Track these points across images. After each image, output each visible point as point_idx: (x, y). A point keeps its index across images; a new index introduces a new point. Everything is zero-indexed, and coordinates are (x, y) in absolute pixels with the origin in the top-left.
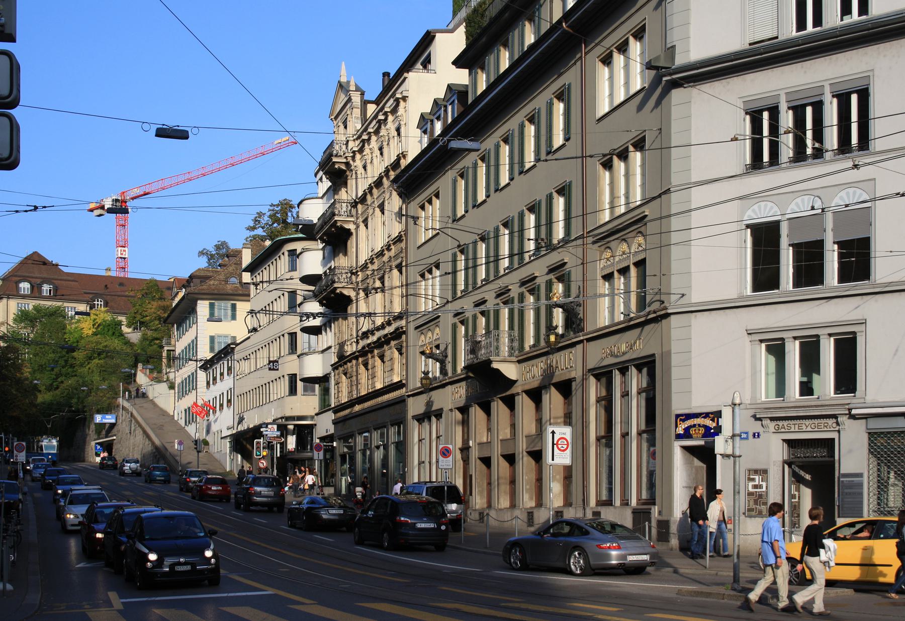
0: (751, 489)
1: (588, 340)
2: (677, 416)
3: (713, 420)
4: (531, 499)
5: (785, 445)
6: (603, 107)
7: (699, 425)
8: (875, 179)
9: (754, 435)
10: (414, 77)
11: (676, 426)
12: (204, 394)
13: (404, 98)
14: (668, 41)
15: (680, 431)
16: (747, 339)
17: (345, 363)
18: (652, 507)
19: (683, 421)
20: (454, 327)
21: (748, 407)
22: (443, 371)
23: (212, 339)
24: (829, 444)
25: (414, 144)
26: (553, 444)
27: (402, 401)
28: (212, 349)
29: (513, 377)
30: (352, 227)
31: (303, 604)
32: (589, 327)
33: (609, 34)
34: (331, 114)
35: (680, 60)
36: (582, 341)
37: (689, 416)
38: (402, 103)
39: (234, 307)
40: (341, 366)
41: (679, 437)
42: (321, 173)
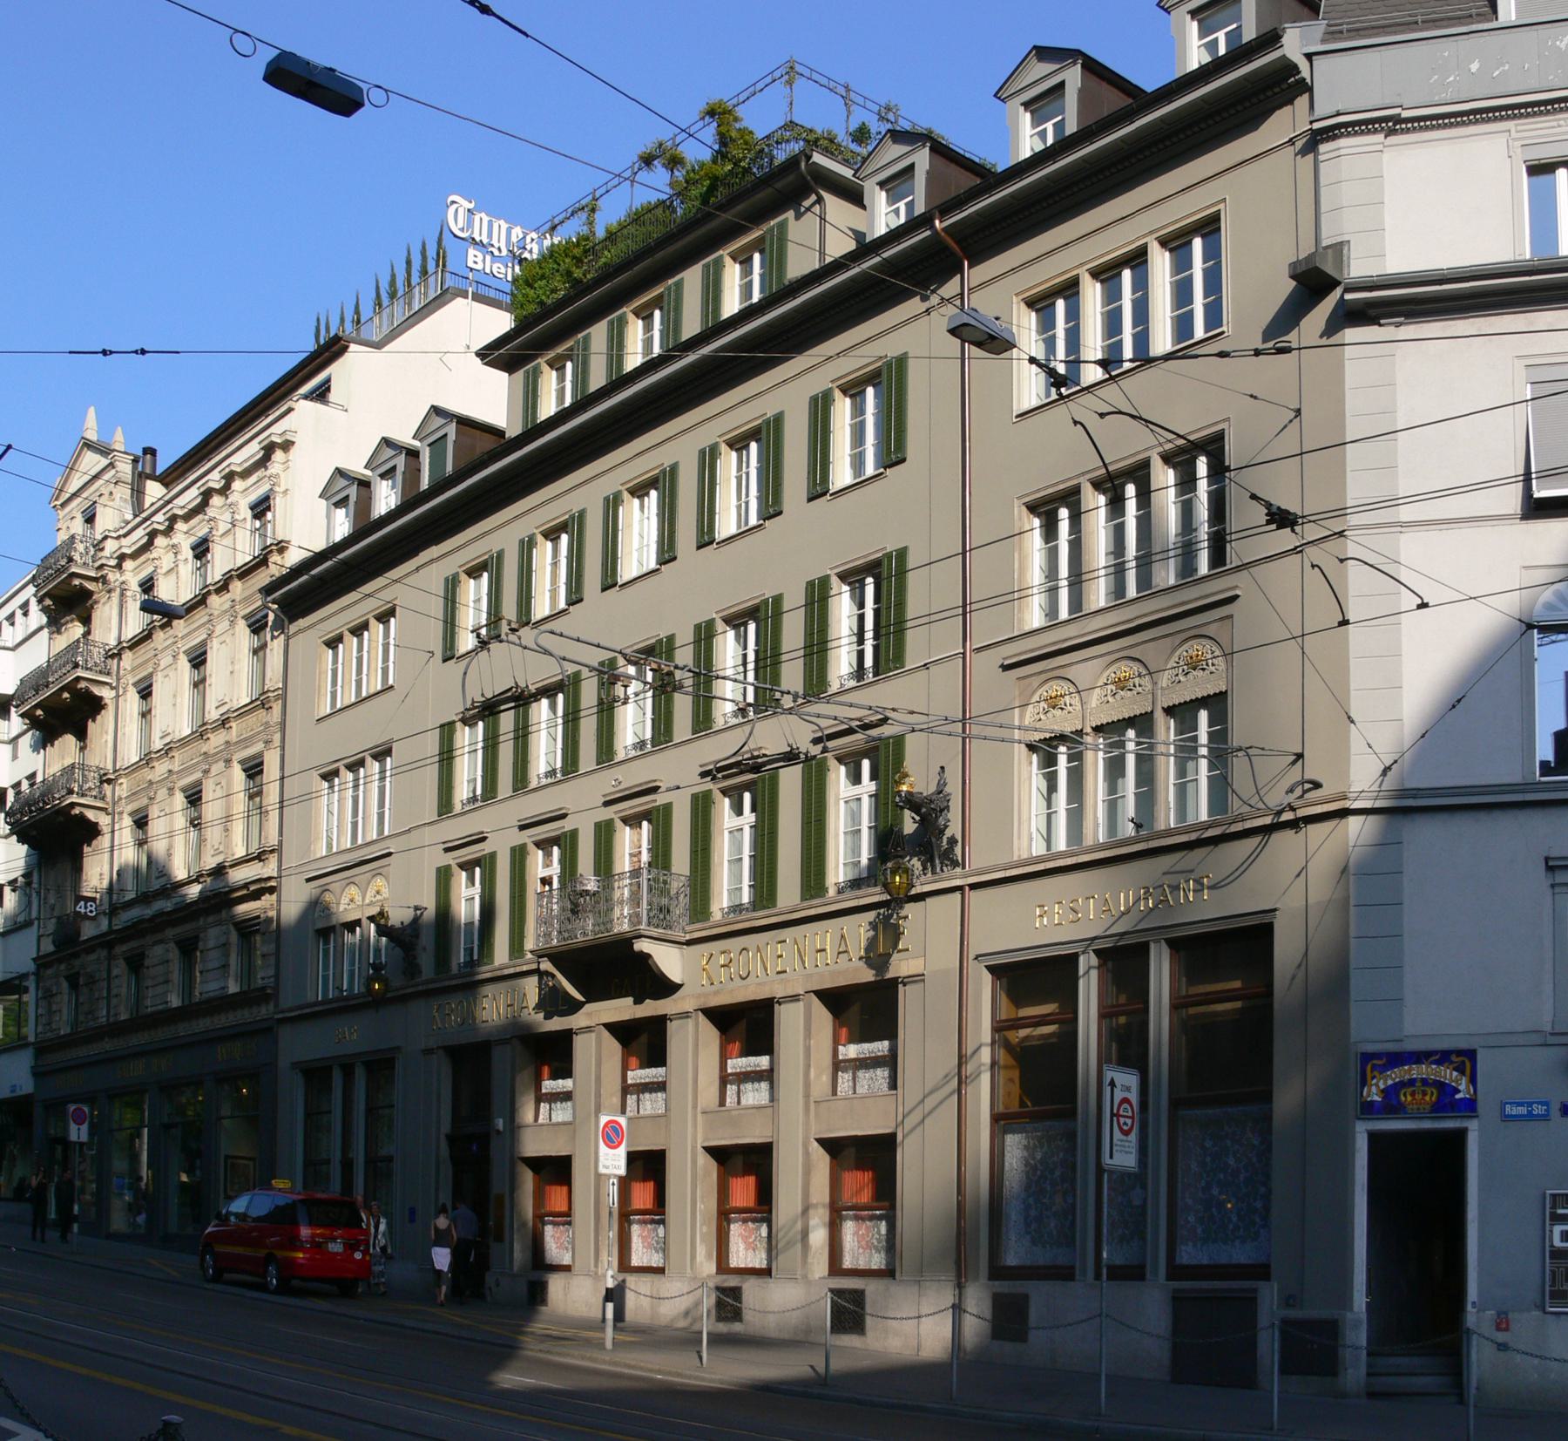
0: (1557, 1243)
1: (973, 887)
2: (1366, 1058)
3: (1460, 1069)
4: (709, 1256)
5: (713, 1165)
7: (1425, 1082)
10: (301, 416)
11: (1364, 1082)
14: (1325, 233)
17: (75, 955)
18: (1261, 1284)
19: (1383, 1069)
21: (1552, 1040)
25: (310, 528)
26: (1112, 1115)
27: (266, 1031)
29: (677, 980)
35: (1359, 267)
36: (960, 888)
37: (1396, 1059)
38: (278, 455)
40: (60, 961)
41: (1368, 1110)
42: (31, 589)
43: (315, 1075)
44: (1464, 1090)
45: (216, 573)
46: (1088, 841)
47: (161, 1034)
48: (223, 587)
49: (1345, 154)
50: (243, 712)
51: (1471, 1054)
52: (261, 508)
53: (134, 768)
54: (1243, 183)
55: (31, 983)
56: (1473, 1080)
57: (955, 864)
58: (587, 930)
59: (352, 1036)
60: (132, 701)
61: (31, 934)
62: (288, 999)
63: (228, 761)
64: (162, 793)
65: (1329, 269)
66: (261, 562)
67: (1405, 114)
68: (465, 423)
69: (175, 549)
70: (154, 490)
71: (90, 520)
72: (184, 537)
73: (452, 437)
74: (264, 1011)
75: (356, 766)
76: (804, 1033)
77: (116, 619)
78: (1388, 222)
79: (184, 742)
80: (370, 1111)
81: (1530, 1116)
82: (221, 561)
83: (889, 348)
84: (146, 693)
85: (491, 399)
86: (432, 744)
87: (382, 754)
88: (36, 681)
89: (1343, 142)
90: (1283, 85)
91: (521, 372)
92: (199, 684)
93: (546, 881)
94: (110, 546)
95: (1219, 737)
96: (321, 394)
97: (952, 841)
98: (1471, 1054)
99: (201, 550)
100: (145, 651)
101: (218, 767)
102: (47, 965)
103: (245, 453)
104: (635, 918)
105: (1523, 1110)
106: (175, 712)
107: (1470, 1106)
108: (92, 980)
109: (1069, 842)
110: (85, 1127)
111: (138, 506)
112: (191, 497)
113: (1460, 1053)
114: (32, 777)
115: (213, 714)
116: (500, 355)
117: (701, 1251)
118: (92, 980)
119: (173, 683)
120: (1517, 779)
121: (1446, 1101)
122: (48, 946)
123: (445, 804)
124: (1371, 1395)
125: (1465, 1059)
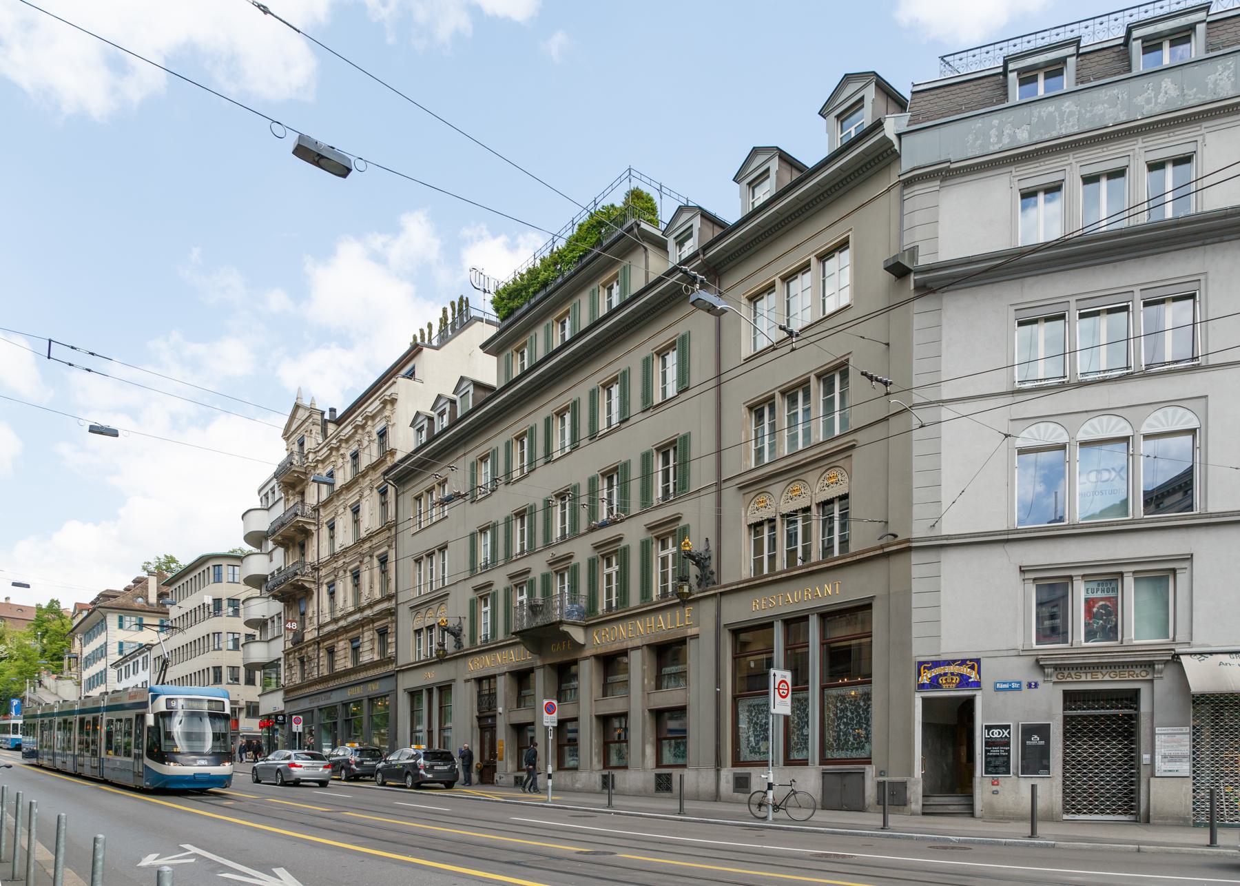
2: (921, 663)
3: (972, 668)
4: (599, 762)
6: (747, 351)
7: (952, 674)
8: (1206, 396)
9: (1030, 686)
10: (401, 386)
11: (919, 675)
13: (393, 401)
15: (925, 679)
16: (1017, 576)
18: (867, 767)
19: (929, 669)
22: (459, 644)
23: (121, 644)
24: (1132, 697)
27: (393, 675)
28: (121, 652)
30: (312, 528)
32: (727, 578)
37: (936, 664)
41: (922, 687)
42: (275, 481)
43: (414, 694)
44: (974, 676)
45: (362, 467)
47: (344, 681)
50: (378, 533)
51: (978, 661)
52: (383, 434)
53: (328, 563)
55: (282, 662)
56: (979, 673)
57: (714, 583)
59: (432, 676)
60: (325, 531)
62: (401, 661)
63: (371, 556)
64: (341, 573)
65: (906, 263)
66: (381, 462)
67: (953, 166)
70: (331, 428)
71: (302, 445)
72: (347, 451)
73: (471, 392)
74: (391, 667)
75: (430, 555)
76: (639, 667)
80: (440, 708)
81: (1010, 689)
82: (365, 462)
85: (488, 370)
87: (443, 549)
88: (280, 524)
89: (917, 187)
90: (885, 156)
91: (505, 354)
92: (356, 522)
93: (521, 602)
94: (311, 456)
95: (844, 516)
96: (411, 375)
97: (712, 573)
98: (978, 661)
99: (355, 456)
100: (330, 508)
101: (367, 559)
102: (288, 654)
103: (373, 406)
105: (1007, 686)
106: (344, 537)
107: (977, 684)
108: (310, 659)
109: (841, 551)
110: (301, 725)
111: (325, 437)
113: (971, 660)
114: (279, 569)
116: (492, 347)
117: (595, 760)
118: (310, 659)
120: (1005, 528)
121: (964, 681)
123: (473, 568)
124: (924, 814)
125: (975, 663)
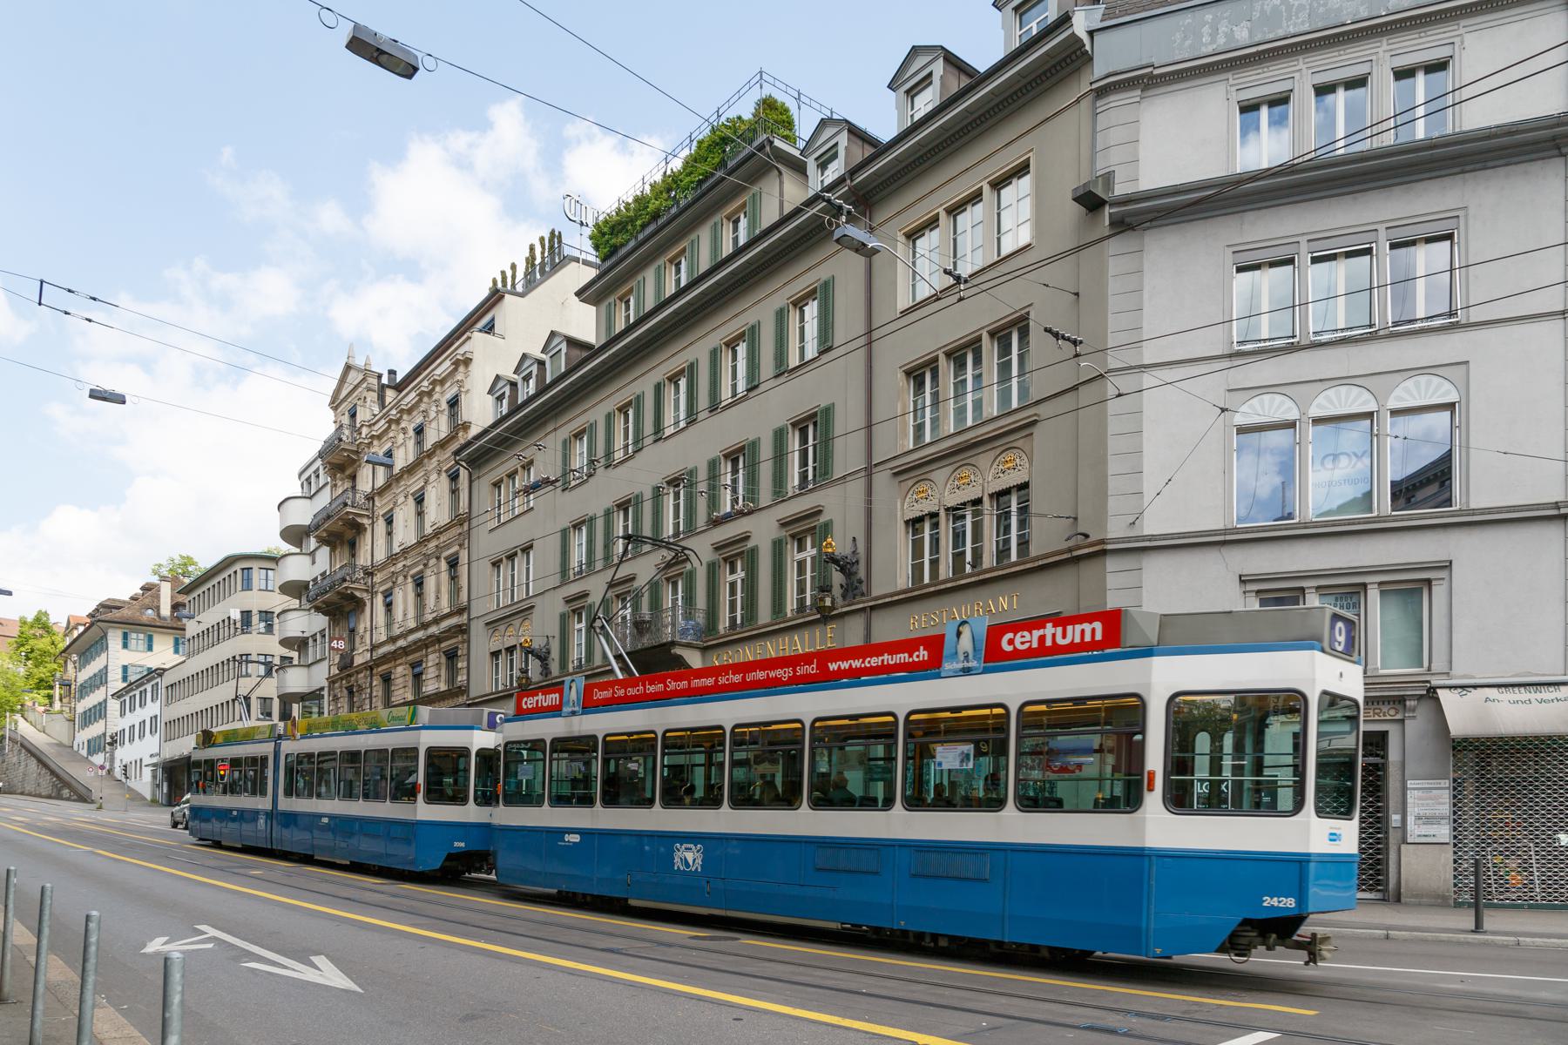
6: (903, 302)
12: (116, 721)
13: (467, 362)
20: (564, 619)
23: (125, 668)
28: (125, 679)
31: (285, 967)
32: (879, 588)
33: (826, 259)
34: (332, 402)
39: (150, 639)
42: (319, 462)
45: (428, 445)
46: (942, 577)
48: (430, 454)
49: (1117, 108)
50: (447, 527)
52: (454, 403)
53: (383, 566)
54: (1059, 142)
55: (325, 693)
58: (646, 641)
60: (381, 526)
61: (325, 664)
63: (438, 558)
65: (1099, 191)
68: (572, 342)
69: (404, 430)
70: (390, 395)
71: (353, 416)
72: (409, 424)
73: (564, 351)
75: (511, 557)
77: (368, 479)
78: (1142, 155)
79: (412, 548)
82: (431, 438)
83: (822, 273)
84: (389, 521)
85: (585, 324)
86: (556, 541)
87: (527, 549)
88: (326, 516)
92: (420, 514)
95: (1023, 511)
96: (490, 329)
97: (860, 582)
99: (419, 431)
100: (388, 497)
101: (433, 561)
104: (673, 634)
106: (405, 533)
108: (360, 689)
111: (383, 406)
112: (412, 397)
115: (429, 530)
118: (360, 689)
119: (405, 515)
122: (335, 671)
